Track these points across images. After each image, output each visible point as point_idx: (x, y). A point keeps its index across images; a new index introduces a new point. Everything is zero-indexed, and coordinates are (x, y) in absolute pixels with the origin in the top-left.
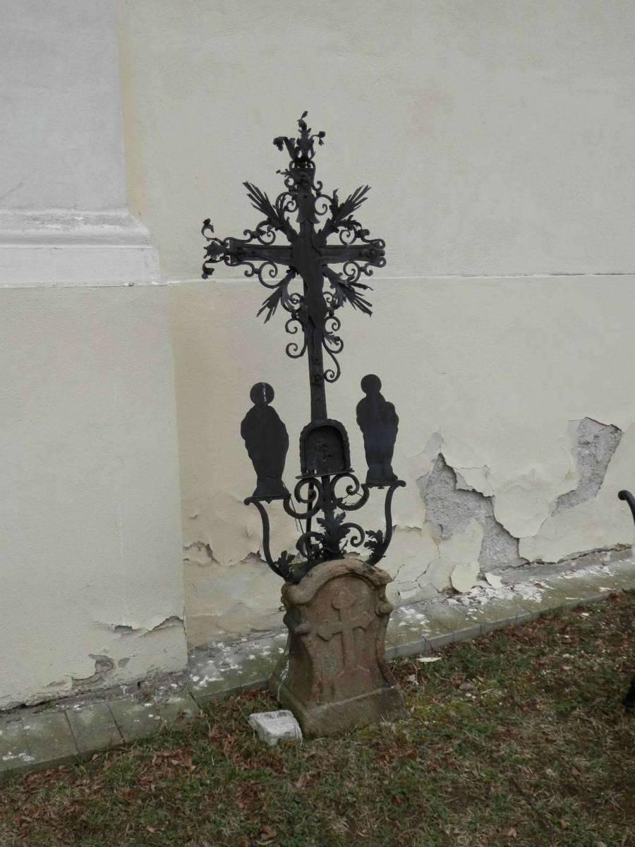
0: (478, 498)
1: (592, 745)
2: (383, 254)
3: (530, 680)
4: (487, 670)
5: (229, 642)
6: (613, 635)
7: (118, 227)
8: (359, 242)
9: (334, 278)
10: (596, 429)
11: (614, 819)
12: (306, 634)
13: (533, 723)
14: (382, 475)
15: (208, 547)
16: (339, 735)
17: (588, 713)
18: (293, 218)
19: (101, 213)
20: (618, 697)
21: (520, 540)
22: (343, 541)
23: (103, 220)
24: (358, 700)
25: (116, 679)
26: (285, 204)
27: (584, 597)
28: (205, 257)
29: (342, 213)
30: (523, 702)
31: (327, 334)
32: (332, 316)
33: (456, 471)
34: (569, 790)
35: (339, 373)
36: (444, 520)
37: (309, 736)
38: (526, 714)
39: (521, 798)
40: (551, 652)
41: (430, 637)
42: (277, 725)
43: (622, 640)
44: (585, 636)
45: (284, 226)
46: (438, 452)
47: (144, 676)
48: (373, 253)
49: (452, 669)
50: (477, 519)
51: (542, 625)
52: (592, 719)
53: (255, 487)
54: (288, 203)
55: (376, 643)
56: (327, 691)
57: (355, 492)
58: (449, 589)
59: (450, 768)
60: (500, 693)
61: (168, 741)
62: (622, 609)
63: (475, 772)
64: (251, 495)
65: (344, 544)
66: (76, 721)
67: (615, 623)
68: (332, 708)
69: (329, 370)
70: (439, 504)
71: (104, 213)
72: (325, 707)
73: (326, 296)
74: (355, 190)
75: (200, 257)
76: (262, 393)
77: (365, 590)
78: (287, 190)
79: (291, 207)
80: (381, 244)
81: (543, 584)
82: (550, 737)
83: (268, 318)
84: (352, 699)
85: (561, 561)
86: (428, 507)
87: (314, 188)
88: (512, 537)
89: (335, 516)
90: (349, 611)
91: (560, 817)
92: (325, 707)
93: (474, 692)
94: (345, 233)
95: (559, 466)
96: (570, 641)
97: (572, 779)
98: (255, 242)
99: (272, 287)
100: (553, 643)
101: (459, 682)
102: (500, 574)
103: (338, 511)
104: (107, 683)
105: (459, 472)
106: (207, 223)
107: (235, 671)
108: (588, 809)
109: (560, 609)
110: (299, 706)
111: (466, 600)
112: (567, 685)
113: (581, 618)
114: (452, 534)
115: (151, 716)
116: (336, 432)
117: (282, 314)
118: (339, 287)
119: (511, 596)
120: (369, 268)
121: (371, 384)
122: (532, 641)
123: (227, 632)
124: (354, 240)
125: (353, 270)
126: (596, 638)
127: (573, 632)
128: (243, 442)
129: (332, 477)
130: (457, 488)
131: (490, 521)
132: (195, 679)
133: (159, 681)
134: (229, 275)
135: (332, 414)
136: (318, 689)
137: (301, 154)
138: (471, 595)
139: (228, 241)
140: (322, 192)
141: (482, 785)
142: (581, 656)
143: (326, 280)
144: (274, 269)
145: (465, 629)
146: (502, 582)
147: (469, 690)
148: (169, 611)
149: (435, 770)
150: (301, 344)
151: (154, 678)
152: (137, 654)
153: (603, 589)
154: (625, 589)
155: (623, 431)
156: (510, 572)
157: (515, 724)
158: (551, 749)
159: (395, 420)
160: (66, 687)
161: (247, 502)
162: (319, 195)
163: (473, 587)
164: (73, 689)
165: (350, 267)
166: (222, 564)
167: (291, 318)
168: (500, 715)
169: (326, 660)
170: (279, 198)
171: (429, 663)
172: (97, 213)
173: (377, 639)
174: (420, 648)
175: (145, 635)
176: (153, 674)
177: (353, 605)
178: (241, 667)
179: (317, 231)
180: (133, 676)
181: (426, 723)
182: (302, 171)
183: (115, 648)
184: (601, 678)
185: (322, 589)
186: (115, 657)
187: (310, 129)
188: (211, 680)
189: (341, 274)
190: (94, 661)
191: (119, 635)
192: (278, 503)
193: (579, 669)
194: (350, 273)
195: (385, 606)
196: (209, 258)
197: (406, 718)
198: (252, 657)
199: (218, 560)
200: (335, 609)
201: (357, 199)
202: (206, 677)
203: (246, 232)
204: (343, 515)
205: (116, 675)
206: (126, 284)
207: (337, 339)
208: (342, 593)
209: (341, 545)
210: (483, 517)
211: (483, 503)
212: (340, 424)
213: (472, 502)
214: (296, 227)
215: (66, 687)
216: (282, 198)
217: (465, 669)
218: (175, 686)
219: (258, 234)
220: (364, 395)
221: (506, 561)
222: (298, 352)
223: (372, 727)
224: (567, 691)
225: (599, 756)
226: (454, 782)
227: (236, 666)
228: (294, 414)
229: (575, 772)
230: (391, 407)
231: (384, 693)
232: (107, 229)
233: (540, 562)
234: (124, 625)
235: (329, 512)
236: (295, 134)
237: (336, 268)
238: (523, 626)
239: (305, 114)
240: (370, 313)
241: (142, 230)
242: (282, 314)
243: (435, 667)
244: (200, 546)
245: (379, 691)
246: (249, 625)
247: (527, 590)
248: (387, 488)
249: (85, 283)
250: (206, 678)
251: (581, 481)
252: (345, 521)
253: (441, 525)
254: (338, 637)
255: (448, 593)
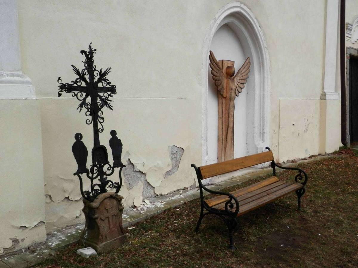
0: (141, 174)
1: (188, 243)
2: (116, 90)
3: (165, 229)
4: (151, 228)
5: (59, 231)
6: (187, 214)
7: (19, 78)
8: (108, 86)
9: (101, 97)
10: (176, 149)
11: (199, 260)
12: (97, 218)
13: (169, 240)
14: (118, 163)
15: (50, 196)
16: (109, 252)
17: (185, 236)
18: (87, 77)
19: (11, 73)
20: (193, 230)
21: (155, 188)
22: (107, 186)
23: (13, 75)
24: (114, 240)
25: (20, 247)
26: (85, 73)
27: (176, 204)
28: (59, 90)
29: (103, 75)
30: (165, 235)
31: (99, 117)
32: (100, 110)
33: (134, 164)
34: (185, 255)
35: (103, 130)
36: (131, 182)
37: (99, 254)
38: (167, 238)
39: (171, 259)
40: (170, 221)
41: (130, 221)
42: (88, 252)
43: (190, 215)
44: (179, 216)
45: (85, 80)
46: (128, 158)
47: (31, 245)
48: (112, 90)
49: (140, 230)
50: (141, 181)
51: (165, 214)
52: (187, 237)
53: (77, 169)
54: (85, 73)
55: (119, 220)
56: (104, 238)
57: (110, 170)
58: (133, 206)
59: (148, 255)
60: (157, 234)
61: (49, 263)
62: (189, 206)
63: (156, 255)
64: (76, 172)
65: (108, 188)
66: (8, 263)
67: (187, 210)
68: (106, 243)
69: (100, 129)
70: (129, 176)
71: (13, 73)
72: (104, 243)
73: (98, 104)
74: (106, 69)
75: (57, 90)
76: (78, 136)
77: (115, 202)
78: (85, 68)
79: (87, 74)
80: (115, 87)
81: (163, 202)
82: (176, 243)
83: (80, 111)
84: (112, 240)
85: (167, 194)
86: (126, 177)
87: (94, 68)
88: (152, 187)
89: (104, 178)
90: (111, 209)
91: (184, 262)
92: (104, 243)
93: (148, 236)
94: (104, 83)
95: (165, 162)
96: (175, 217)
97: (185, 252)
98: (75, 85)
99: (81, 100)
100: (170, 218)
101: (143, 233)
102: (149, 200)
103: (105, 176)
104: (17, 249)
105: (135, 165)
106: (59, 78)
107: (64, 240)
108: (191, 259)
109: (170, 208)
110: (95, 245)
111: (139, 209)
112: (177, 229)
113: (177, 210)
114: (133, 187)
115: (38, 257)
116: (103, 149)
117: (84, 110)
118: (102, 101)
119: (153, 206)
120: (112, 94)
121: (113, 133)
122: (163, 219)
123: (58, 227)
124: (106, 85)
125: (107, 95)
126: (183, 216)
127: (175, 215)
128: (73, 153)
129: (102, 165)
130: (135, 170)
131: (145, 182)
132: (50, 244)
133: (36, 246)
134: (67, 96)
135: (102, 143)
136: (101, 237)
137: (89, 56)
138: (141, 207)
139: (66, 85)
140: (96, 69)
141: (159, 258)
142: (180, 221)
143: (98, 98)
144: (81, 94)
145: (141, 217)
146: (150, 202)
147: (147, 235)
148: (40, 219)
149: (143, 256)
150: (91, 120)
151: (34, 245)
152: (28, 237)
153: (182, 201)
154: (189, 201)
155: (184, 149)
156: (153, 199)
157: (164, 241)
158: (177, 246)
159: (121, 145)
160: (1, 252)
161: (75, 174)
162: (95, 70)
163: (141, 205)
164: (3, 252)
165: (106, 94)
166: (55, 202)
167: (87, 111)
168: (159, 240)
169: (104, 227)
170: (82, 70)
171: (132, 229)
172: (10, 73)
173: (119, 219)
174: (128, 225)
175: (31, 229)
176: (34, 244)
177: (112, 207)
178: (66, 238)
179: (95, 82)
180: (26, 245)
181: (136, 245)
182: (89, 62)
183: (19, 235)
184: (187, 226)
185: (102, 203)
186: (19, 238)
187: (92, 48)
188: (56, 243)
189: (103, 96)
190: (12, 241)
191: (21, 230)
192: (85, 174)
193: (179, 224)
194: (106, 96)
195: (121, 207)
196: (60, 90)
197: (130, 245)
198: (69, 235)
199: (54, 201)
200: (106, 209)
201: (108, 71)
202: (54, 243)
203: (72, 82)
204: (107, 178)
205: (20, 246)
206: (24, 99)
207: (103, 118)
208: (108, 203)
209: (106, 188)
210: (143, 180)
211: (143, 175)
212: (104, 147)
213: (139, 175)
214: (88, 80)
215: (1, 252)
216: (84, 70)
217: (144, 229)
218: (43, 247)
219: (76, 82)
220: (111, 137)
221: (151, 195)
222: (90, 123)
223: (119, 249)
224: (177, 230)
225: (191, 246)
226: (150, 259)
227: (64, 238)
228: (89, 144)
229: (185, 251)
230: (120, 141)
231: (122, 237)
232: (16, 78)
233: (161, 195)
234: (23, 226)
235: (102, 177)
236: (88, 50)
237: (101, 94)
238: (160, 215)
239: (91, 43)
240: (112, 109)
241: (28, 79)
242: (84, 110)
243: (134, 230)
244: (47, 195)
245: (121, 236)
246: (65, 224)
247: (158, 204)
248: (120, 168)
249: (8, 98)
250: (54, 243)
251: (172, 167)
252: (107, 179)
253: (129, 184)
254: (107, 219)
255: (133, 208)
